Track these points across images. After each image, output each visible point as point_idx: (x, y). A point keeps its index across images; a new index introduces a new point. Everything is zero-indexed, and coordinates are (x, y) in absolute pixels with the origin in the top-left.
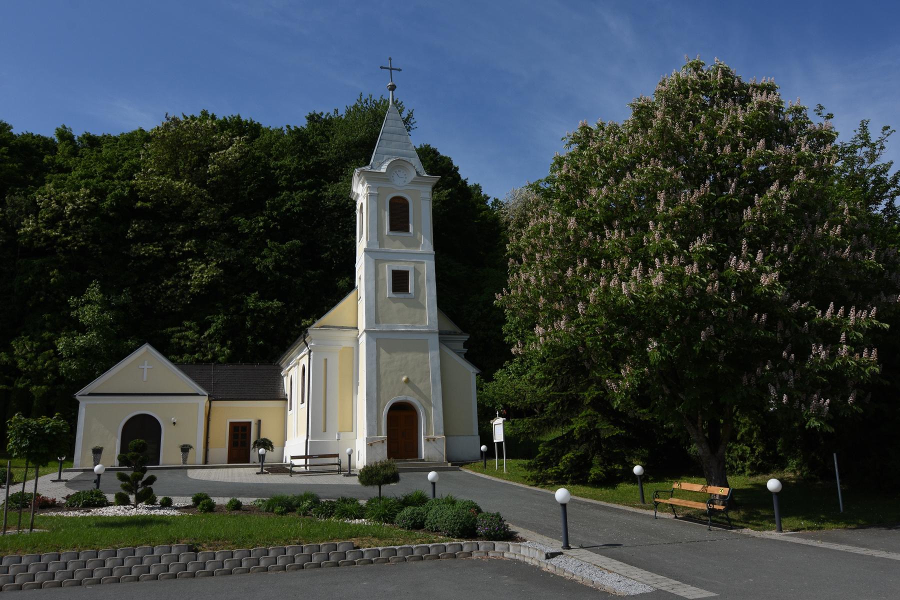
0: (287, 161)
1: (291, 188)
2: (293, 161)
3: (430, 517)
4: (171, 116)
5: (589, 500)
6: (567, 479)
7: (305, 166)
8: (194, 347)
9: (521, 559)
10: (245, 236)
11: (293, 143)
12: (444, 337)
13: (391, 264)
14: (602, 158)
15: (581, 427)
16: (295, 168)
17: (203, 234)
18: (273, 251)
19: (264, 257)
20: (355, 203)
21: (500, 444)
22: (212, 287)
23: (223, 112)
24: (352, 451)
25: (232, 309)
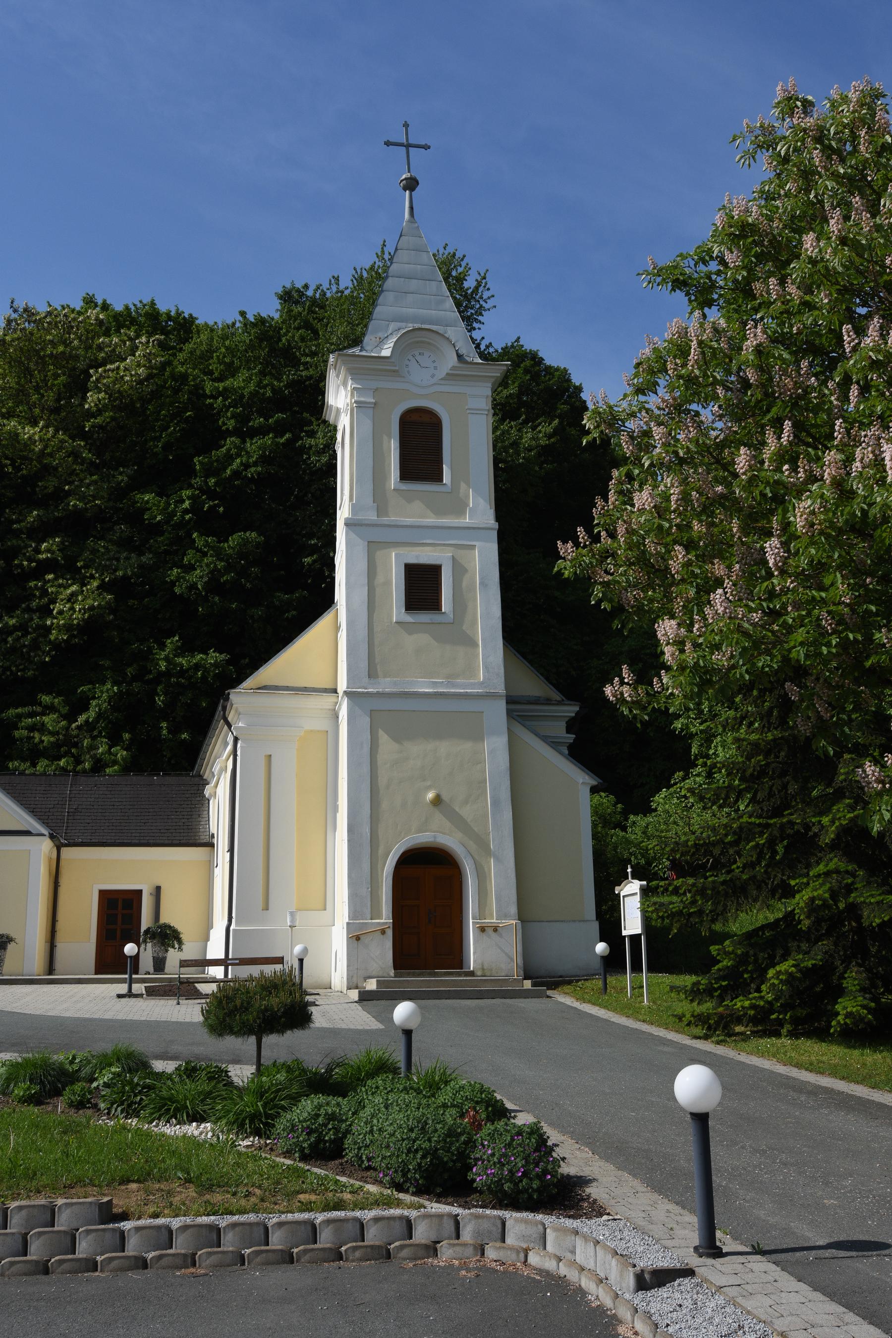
0: (236, 382)
1: (244, 433)
2: (248, 380)
3: (359, 1127)
4: (21, 305)
5: (826, 1081)
6: (780, 1023)
7: (274, 390)
8: (57, 745)
9: (573, 1276)
10: (156, 529)
11: (251, 347)
12: (518, 708)
13: (403, 551)
14: (828, 151)
15: (812, 899)
16: (254, 394)
17: (77, 527)
18: (205, 554)
19: (191, 568)
20: (335, 429)
21: (635, 938)
22: (92, 627)
23: (122, 297)
24: (305, 951)
25: (130, 671)
